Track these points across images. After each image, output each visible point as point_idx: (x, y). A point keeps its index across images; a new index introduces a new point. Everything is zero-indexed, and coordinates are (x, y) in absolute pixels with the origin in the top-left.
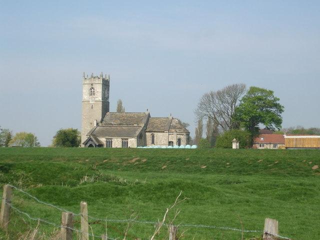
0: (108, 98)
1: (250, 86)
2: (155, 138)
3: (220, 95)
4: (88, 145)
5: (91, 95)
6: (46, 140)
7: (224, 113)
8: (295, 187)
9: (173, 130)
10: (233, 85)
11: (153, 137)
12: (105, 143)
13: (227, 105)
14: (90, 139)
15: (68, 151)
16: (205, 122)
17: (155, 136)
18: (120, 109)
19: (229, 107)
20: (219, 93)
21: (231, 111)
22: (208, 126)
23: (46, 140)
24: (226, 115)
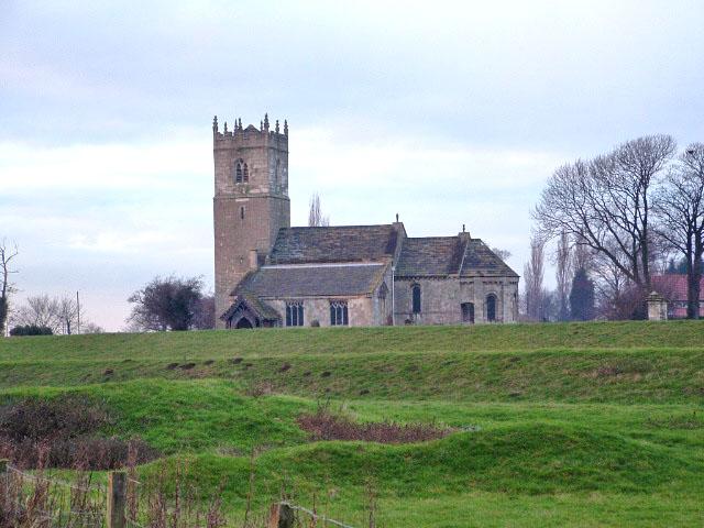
0: (287, 186)
1: (37, 292)
2: (422, 296)
3: (602, 169)
4: (236, 320)
5: (239, 180)
6: (113, 314)
7: (613, 216)
8: (387, 491)
9: (473, 272)
10: (640, 140)
11: (417, 293)
12: (283, 313)
13: (624, 195)
14: (242, 306)
15: (174, 344)
16: (551, 247)
17: (422, 288)
18: (315, 211)
19: (630, 199)
20: (600, 163)
21: (627, 212)
22: (563, 255)
23: (113, 314)
24: (619, 220)
